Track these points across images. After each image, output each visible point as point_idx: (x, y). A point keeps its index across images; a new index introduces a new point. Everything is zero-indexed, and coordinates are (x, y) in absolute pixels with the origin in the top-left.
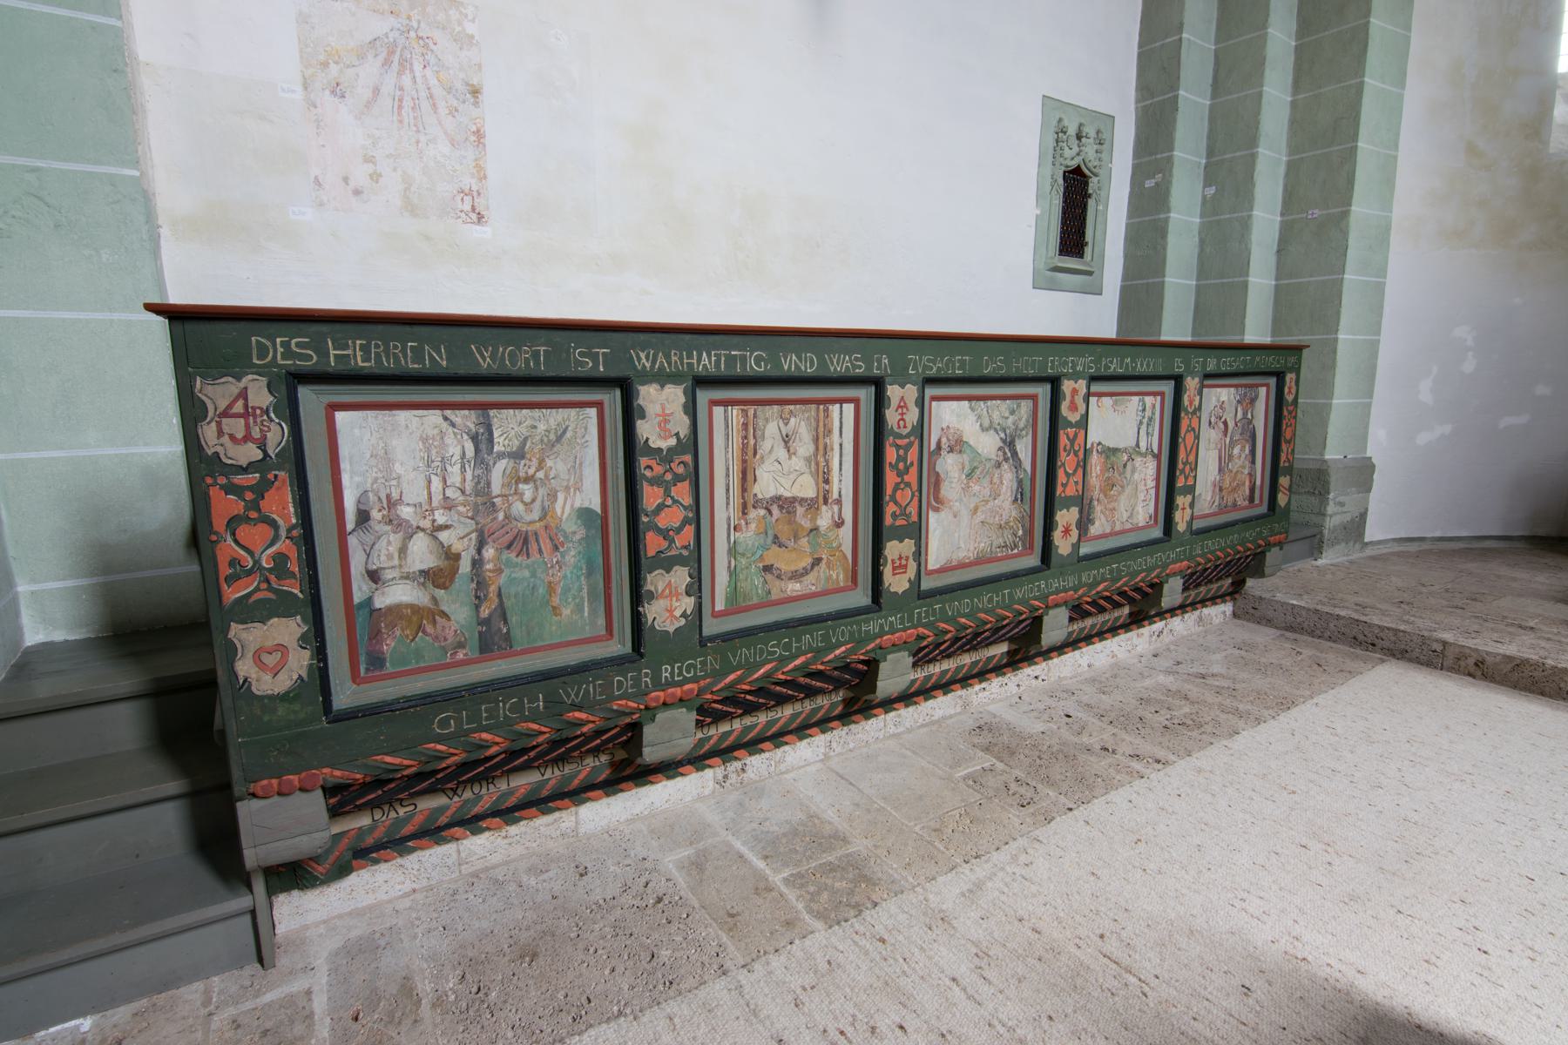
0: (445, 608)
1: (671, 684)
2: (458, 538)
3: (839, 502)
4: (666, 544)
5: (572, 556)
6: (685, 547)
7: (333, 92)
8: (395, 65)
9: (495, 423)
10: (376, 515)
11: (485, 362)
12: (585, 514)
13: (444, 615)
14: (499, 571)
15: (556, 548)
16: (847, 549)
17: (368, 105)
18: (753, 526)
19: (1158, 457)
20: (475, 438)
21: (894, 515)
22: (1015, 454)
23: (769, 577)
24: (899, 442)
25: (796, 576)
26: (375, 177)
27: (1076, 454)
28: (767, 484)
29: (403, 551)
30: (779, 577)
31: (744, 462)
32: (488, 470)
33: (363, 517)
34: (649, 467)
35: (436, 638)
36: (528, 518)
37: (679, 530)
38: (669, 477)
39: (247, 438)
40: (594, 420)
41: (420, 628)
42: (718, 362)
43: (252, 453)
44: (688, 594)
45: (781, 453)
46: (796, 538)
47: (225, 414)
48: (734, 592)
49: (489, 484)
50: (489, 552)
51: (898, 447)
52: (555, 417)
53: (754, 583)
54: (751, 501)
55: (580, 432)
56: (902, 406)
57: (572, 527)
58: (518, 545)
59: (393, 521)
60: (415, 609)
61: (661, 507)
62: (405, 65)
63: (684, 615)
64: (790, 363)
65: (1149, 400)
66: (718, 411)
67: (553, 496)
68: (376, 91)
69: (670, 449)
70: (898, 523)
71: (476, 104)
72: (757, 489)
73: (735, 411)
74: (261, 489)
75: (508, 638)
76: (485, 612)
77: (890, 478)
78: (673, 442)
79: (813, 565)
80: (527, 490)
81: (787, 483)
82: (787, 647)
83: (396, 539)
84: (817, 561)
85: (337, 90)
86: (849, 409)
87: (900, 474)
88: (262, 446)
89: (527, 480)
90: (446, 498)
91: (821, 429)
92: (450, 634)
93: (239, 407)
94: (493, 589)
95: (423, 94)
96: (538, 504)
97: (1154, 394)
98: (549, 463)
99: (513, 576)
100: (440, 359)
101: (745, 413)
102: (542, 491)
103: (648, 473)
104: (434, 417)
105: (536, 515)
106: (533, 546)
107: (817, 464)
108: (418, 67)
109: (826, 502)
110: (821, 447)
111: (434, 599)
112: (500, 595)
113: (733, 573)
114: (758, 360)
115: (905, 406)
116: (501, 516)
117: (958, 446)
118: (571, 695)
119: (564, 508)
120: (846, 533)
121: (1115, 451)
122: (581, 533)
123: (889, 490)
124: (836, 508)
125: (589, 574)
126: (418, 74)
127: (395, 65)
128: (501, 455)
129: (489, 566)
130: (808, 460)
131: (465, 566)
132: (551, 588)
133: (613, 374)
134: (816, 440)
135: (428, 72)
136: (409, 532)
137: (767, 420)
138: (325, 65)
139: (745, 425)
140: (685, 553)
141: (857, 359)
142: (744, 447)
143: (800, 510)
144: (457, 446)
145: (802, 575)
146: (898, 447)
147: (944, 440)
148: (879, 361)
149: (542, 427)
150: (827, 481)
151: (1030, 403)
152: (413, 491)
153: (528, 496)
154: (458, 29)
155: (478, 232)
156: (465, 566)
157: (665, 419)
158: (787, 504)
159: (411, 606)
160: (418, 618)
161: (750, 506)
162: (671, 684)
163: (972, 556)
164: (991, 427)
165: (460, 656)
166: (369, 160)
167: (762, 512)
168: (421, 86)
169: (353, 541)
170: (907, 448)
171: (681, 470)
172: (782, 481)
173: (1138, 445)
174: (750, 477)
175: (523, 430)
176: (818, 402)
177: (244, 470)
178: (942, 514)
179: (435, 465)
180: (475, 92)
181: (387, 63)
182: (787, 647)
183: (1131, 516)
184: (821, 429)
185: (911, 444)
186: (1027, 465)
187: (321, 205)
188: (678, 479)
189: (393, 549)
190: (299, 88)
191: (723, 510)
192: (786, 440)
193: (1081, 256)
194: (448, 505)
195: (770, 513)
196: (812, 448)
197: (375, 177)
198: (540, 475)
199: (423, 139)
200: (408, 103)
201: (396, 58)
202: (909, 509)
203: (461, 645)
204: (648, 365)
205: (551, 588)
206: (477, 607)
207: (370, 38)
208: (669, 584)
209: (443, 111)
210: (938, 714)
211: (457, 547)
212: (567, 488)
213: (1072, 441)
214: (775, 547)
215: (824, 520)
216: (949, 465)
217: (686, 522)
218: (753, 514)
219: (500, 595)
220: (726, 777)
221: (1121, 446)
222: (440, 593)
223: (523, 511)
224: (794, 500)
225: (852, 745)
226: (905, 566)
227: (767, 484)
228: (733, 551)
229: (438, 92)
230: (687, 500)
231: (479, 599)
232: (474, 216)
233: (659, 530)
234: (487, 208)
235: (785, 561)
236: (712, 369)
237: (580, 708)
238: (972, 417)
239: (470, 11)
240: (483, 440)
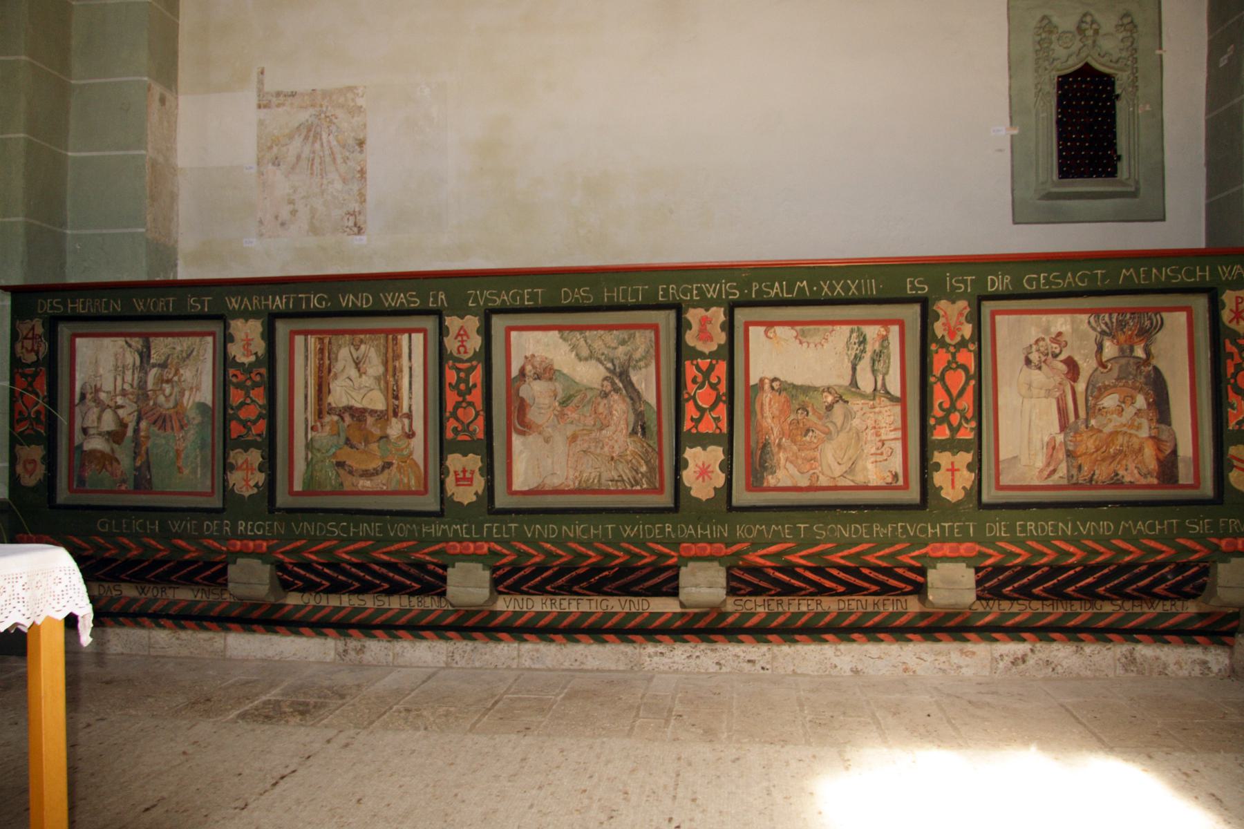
0: (117, 456)
1: (243, 537)
2: (128, 413)
3: (409, 416)
4: (245, 431)
5: (191, 433)
6: (259, 435)
7: (273, 164)
8: (311, 139)
9: (153, 345)
10: (89, 396)
11: (140, 307)
12: (201, 407)
13: (117, 460)
14: (148, 437)
15: (182, 427)
16: (418, 456)
17: (293, 168)
18: (327, 428)
19: (902, 401)
20: (141, 355)
21: (455, 430)
22: (629, 385)
23: (341, 471)
24: (460, 365)
25: (366, 474)
26: (294, 212)
27: (714, 387)
28: (340, 394)
29: (99, 418)
30: (351, 472)
31: (320, 378)
32: (146, 373)
33: (83, 396)
34: (235, 375)
35: (112, 474)
36: (167, 406)
37: (254, 422)
38: (249, 383)
39: (32, 350)
40: (211, 345)
41: (104, 466)
42: (287, 303)
43: (32, 358)
44: (260, 470)
45: (353, 372)
46: (367, 442)
47: (26, 338)
48: (310, 479)
49: (146, 382)
50: (143, 424)
51: (459, 370)
52: (186, 342)
53: (329, 476)
54: (326, 408)
55: (202, 352)
56: (462, 334)
57: (194, 416)
58: (160, 422)
59: (97, 401)
60: (103, 454)
61: (243, 404)
62: (317, 136)
63: (256, 485)
64: (348, 301)
65: (872, 332)
66: (299, 339)
67: (182, 393)
68: (299, 157)
69: (250, 364)
70: (460, 438)
71: (361, 152)
72: (331, 399)
73: (312, 340)
74: (35, 376)
75: (150, 481)
76: (138, 464)
77: (451, 398)
78: (253, 358)
79: (383, 468)
80: (167, 388)
81: (359, 398)
82: (346, 530)
83: (96, 410)
84: (388, 465)
85: (276, 162)
86: (418, 338)
87: (461, 394)
88: (37, 354)
89: (168, 381)
90: (123, 390)
91: (390, 354)
92: (119, 473)
93: (30, 335)
94: (144, 448)
95: (327, 152)
96: (172, 398)
97: (885, 323)
98: (182, 371)
99: (158, 442)
100: (117, 307)
101: (321, 341)
102: (176, 390)
103: (234, 380)
104: (120, 341)
105: (171, 404)
106: (168, 424)
107: (387, 383)
108: (324, 136)
109: (395, 414)
110: (390, 369)
111: (112, 450)
112: (147, 453)
113: (309, 463)
114: (320, 300)
115: (466, 334)
116: (151, 403)
117: (547, 372)
118: (176, 527)
119: (188, 401)
120: (417, 443)
121: (806, 389)
122: (198, 420)
123: (449, 408)
124: (406, 421)
125: (202, 448)
126: (325, 140)
127: (311, 139)
128: (154, 366)
129: (142, 434)
130: (378, 379)
131: (130, 432)
132: (178, 453)
133: (215, 312)
134: (385, 364)
135: (331, 138)
136: (103, 407)
137: (340, 347)
138: (270, 148)
139: (321, 351)
140: (259, 439)
141: (411, 296)
142: (320, 368)
143: (370, 420)
144: (131, 358)
145: (372, 475)
146: (459, 370)
147: (529, 368)
148: (435, 297)
149: (179, 348)
150: (396, 397)
151: (650, 334)
152: (108, 385)
153: (168, 392)
154: (352, 104)
155: (362, 240)
156: (130, 432)
157: (248, 342)
158: (359, 414)
159: (100, 452)
160: (105, 460)
161: (325, 412)
162: (243, 537)
163: (572, 485)
164: (591, 357)
165: (123, 488)
166: (291, 202)
167: (336, 418)
168: (326, 148)
169: (77, 410)
170: (469, 371)
171: (258, 378)
172: (353, 394)
173: (854, 383)
174: (325, 389)
175: (167, 351)
176: (387, 332)
177: (29, 366)
178: (530, 438)
179: (120, 369)
180: (361, 143)
181: (306, 138)
182: (346, 530)
183: (851, 470)
184: (390, 354)
185: (473, 368)
186: (651, 398)
187: (262, 235)
188: (256, 385)
189: (95, 417)
190: (255, 166)
191: (302, 412)
192: (357, 364)
193: (1113, 174)
194: (124, 393)
195: (343, 419)
196: (381, 369)
197: (294, 212)
198: (176, 379)
199: (325, 182)
200: (317, 160)
201: (312, 134)
202: (472, 427)
203: (124, 481)
204: (237, 307)
205: (178, 453)
206: (135, 458)
207: (296, 125)
208: (246, 461)
209: (339, 161)
210: (591, 664)
211: (127, 419)
212: (191, 389)
213: (707, 374)
214: (347, 449)
215: (395, 429)
216: (535, 391)
217: (260, 416)
218: (327, 419)
219: (147, 453)
220: (345, 651)
221: (818, 383)
222: (115, 446)
223: (164, 401)
224: (363, 411)
225: (477, 664)
226: (471, 480)
227: (340, 394)
228: (309, 446)
229: (337, 149)
230: (262, 401)
231: (136, 454)
232: (356, 230)
233: (240, 420)
234: (365, 222)
235: (355, 460)
236: (282, 307)
237: (181, 538)
238: (565, 347)
239: (360, 91)
240: (145, 355)
